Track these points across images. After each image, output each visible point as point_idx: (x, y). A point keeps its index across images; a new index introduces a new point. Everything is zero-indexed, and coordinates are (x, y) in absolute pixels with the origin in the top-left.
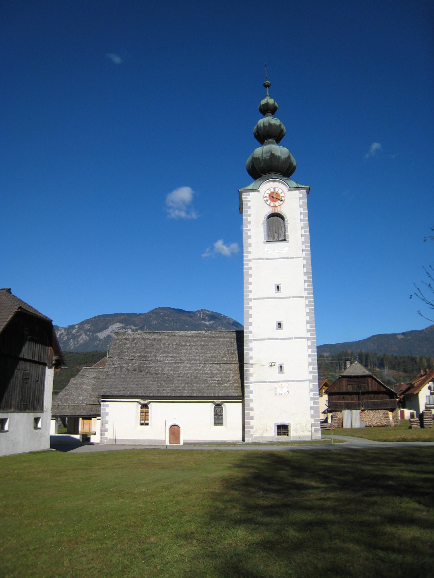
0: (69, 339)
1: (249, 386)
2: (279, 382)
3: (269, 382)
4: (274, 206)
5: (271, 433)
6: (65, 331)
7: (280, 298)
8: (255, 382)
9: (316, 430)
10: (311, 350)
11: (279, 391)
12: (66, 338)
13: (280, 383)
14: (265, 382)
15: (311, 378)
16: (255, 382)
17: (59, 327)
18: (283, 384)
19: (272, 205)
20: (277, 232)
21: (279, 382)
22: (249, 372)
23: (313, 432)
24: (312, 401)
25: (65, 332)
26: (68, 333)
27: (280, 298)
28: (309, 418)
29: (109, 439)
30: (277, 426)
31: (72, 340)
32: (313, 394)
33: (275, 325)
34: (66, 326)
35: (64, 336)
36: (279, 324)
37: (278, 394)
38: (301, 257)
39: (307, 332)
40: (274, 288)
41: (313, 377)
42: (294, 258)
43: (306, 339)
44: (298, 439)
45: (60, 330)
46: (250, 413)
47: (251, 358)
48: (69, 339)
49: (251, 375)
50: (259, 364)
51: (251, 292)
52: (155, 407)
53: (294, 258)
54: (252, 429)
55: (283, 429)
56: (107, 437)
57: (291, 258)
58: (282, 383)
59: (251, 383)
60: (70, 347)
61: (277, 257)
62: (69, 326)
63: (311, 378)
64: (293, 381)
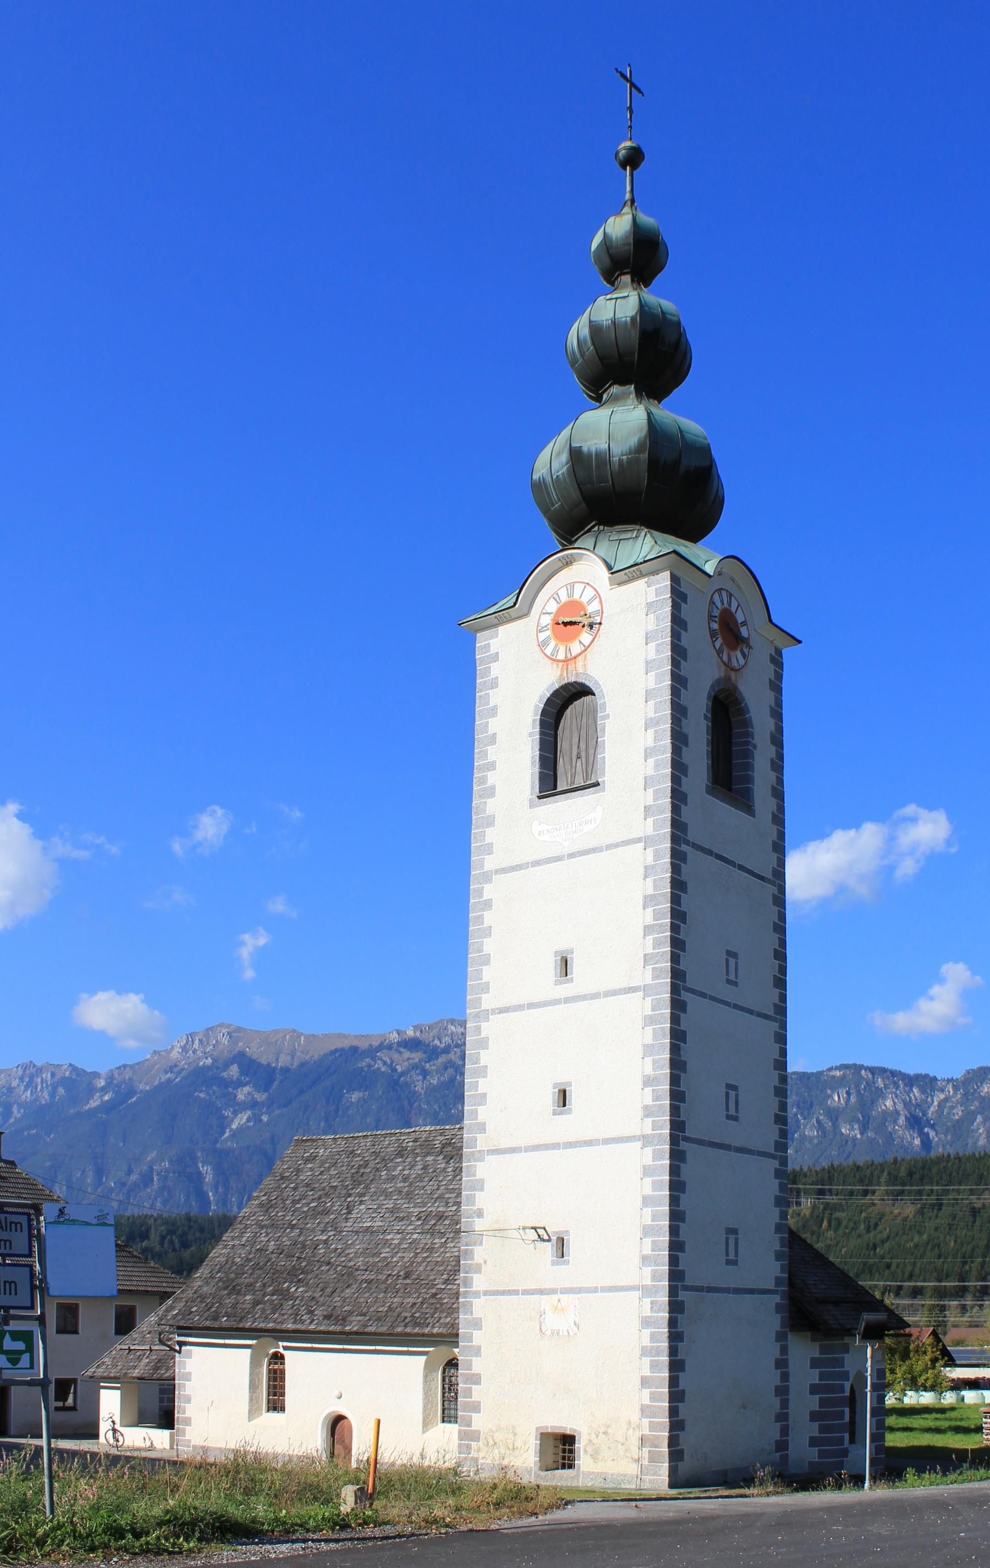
0: (969, 1116)
1: (471, 1303)
2: (553, 1291)
3: (526, 1292)
4: (566, 661)
5: (525, 1461)
6: (956, 1088)
7: (567, 1000)
8: (486, 1293)
9: (653, 1458)
10: (654, 1183)
11: (552, 1321)
12: (958, 1113)
13: (555, 1297)
14: (516, 1292)
15: (648, 1281)
16: (486, 1293)
17: (935, 1079)
18: (564, 1297)
19: (561, 656)
20: (583, 754)
21: (553, 1291)
22: (473, 1259)
23: (646, 1462)
24: (647, 1360)
25: (955, 1093)
26: (965, 1094)
27: (567, 1000)
28: (635, 1416)
29: (195, 1447)
30: (541, 1434)
31: (979, 1118)
32: (652, 1334)
33: (549, 1098)
34: (958, 1074)
35: (952, 1108)
36: (564, 1093)
37: (548, 1333)
38: (639, 840)
39: (646, 1116)
40: (550, 966)
41: (654, 1278)
42: (617, 845)
43: (639, 1144)
44: (598, 1484)
45: (942, 1090)
46: (470, 1389)
47: (480, 1214)
48: (969, 1116)
49: (478, 1269)
50: (499, 1232)
51: (485, 988)
52: (301, 1365)
53: (617, 845)
54: (477, 1440)
55: (561, 1448)
56: (190, 1441)
57: (609, 847)
58: (562, 1296)
59: (477, 1294)
60: (978, 1139)
61: (566, 851)
62: (968, 1072)
63: (648, 1281)
64: (595, 1290)
